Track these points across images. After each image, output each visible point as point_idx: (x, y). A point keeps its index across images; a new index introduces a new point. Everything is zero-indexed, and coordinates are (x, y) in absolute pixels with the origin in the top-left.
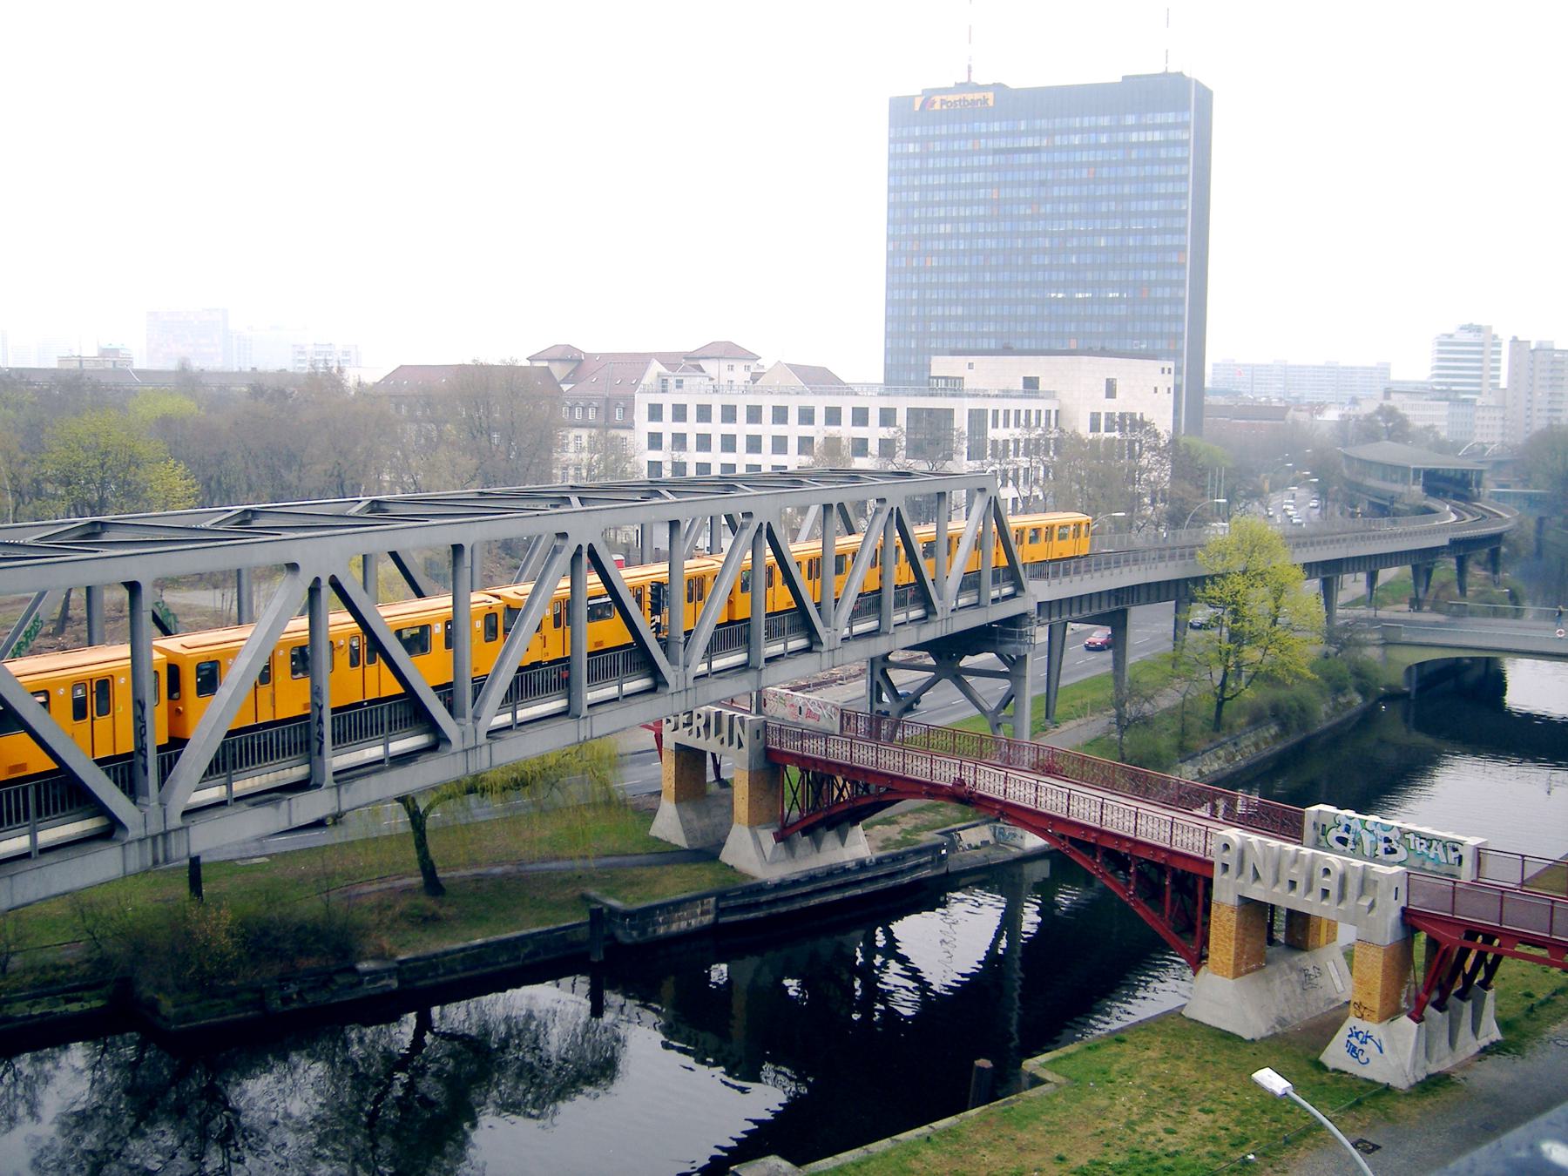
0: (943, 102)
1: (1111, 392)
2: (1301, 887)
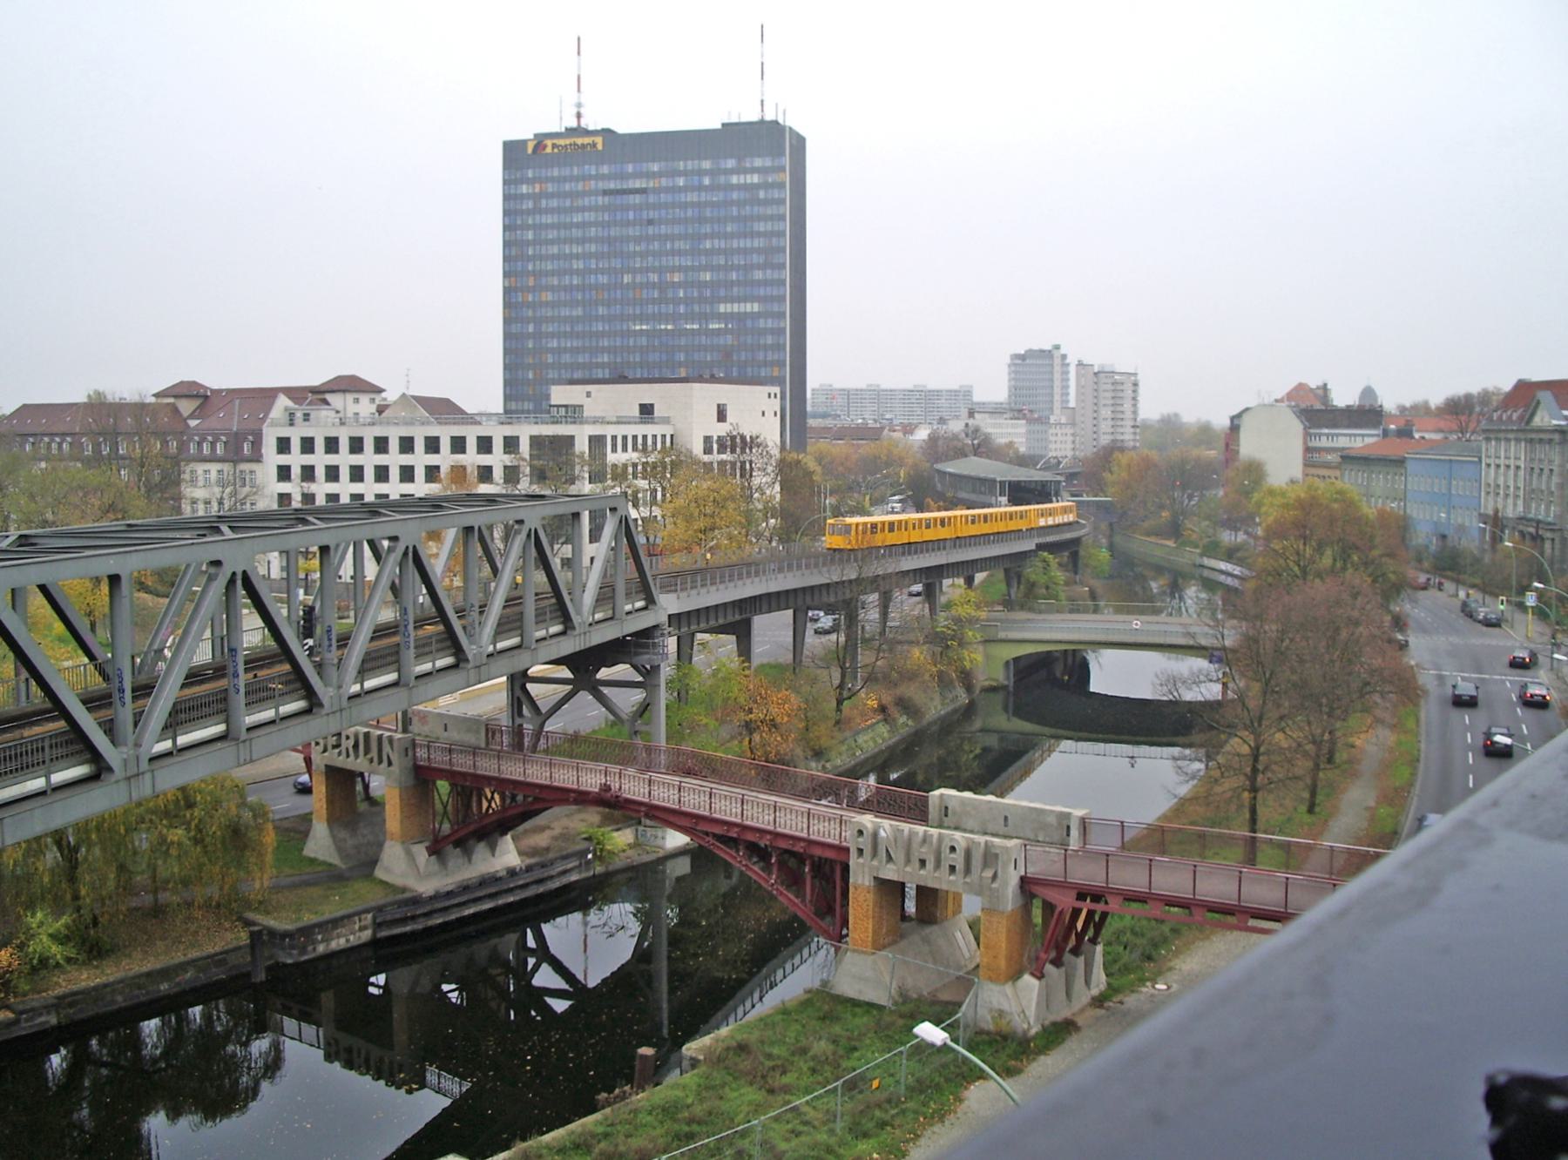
0: (554, 146)
1: (721, 416)
2: (930, 865)
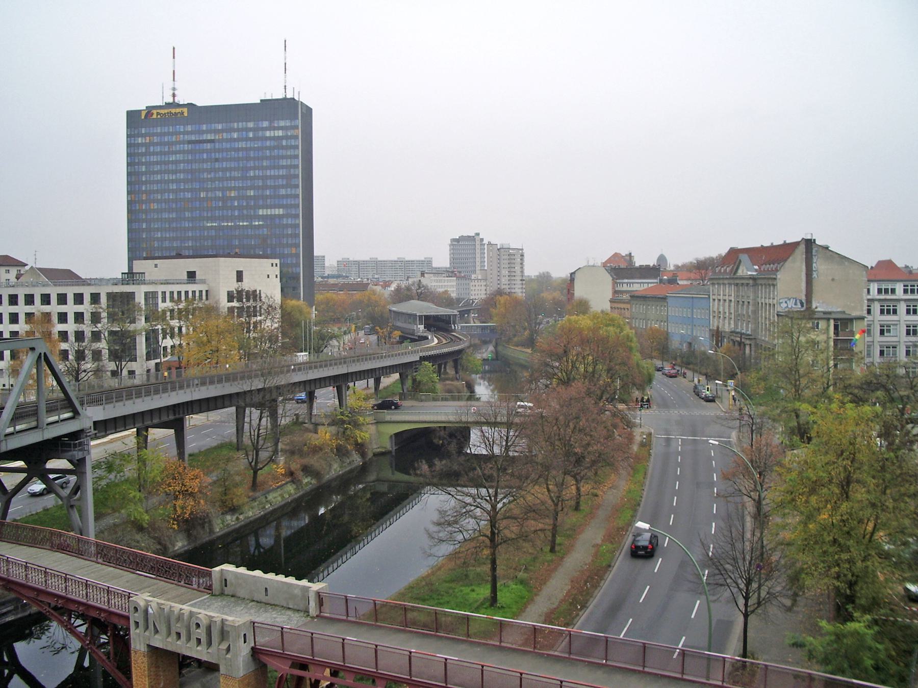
1: (240, 276)
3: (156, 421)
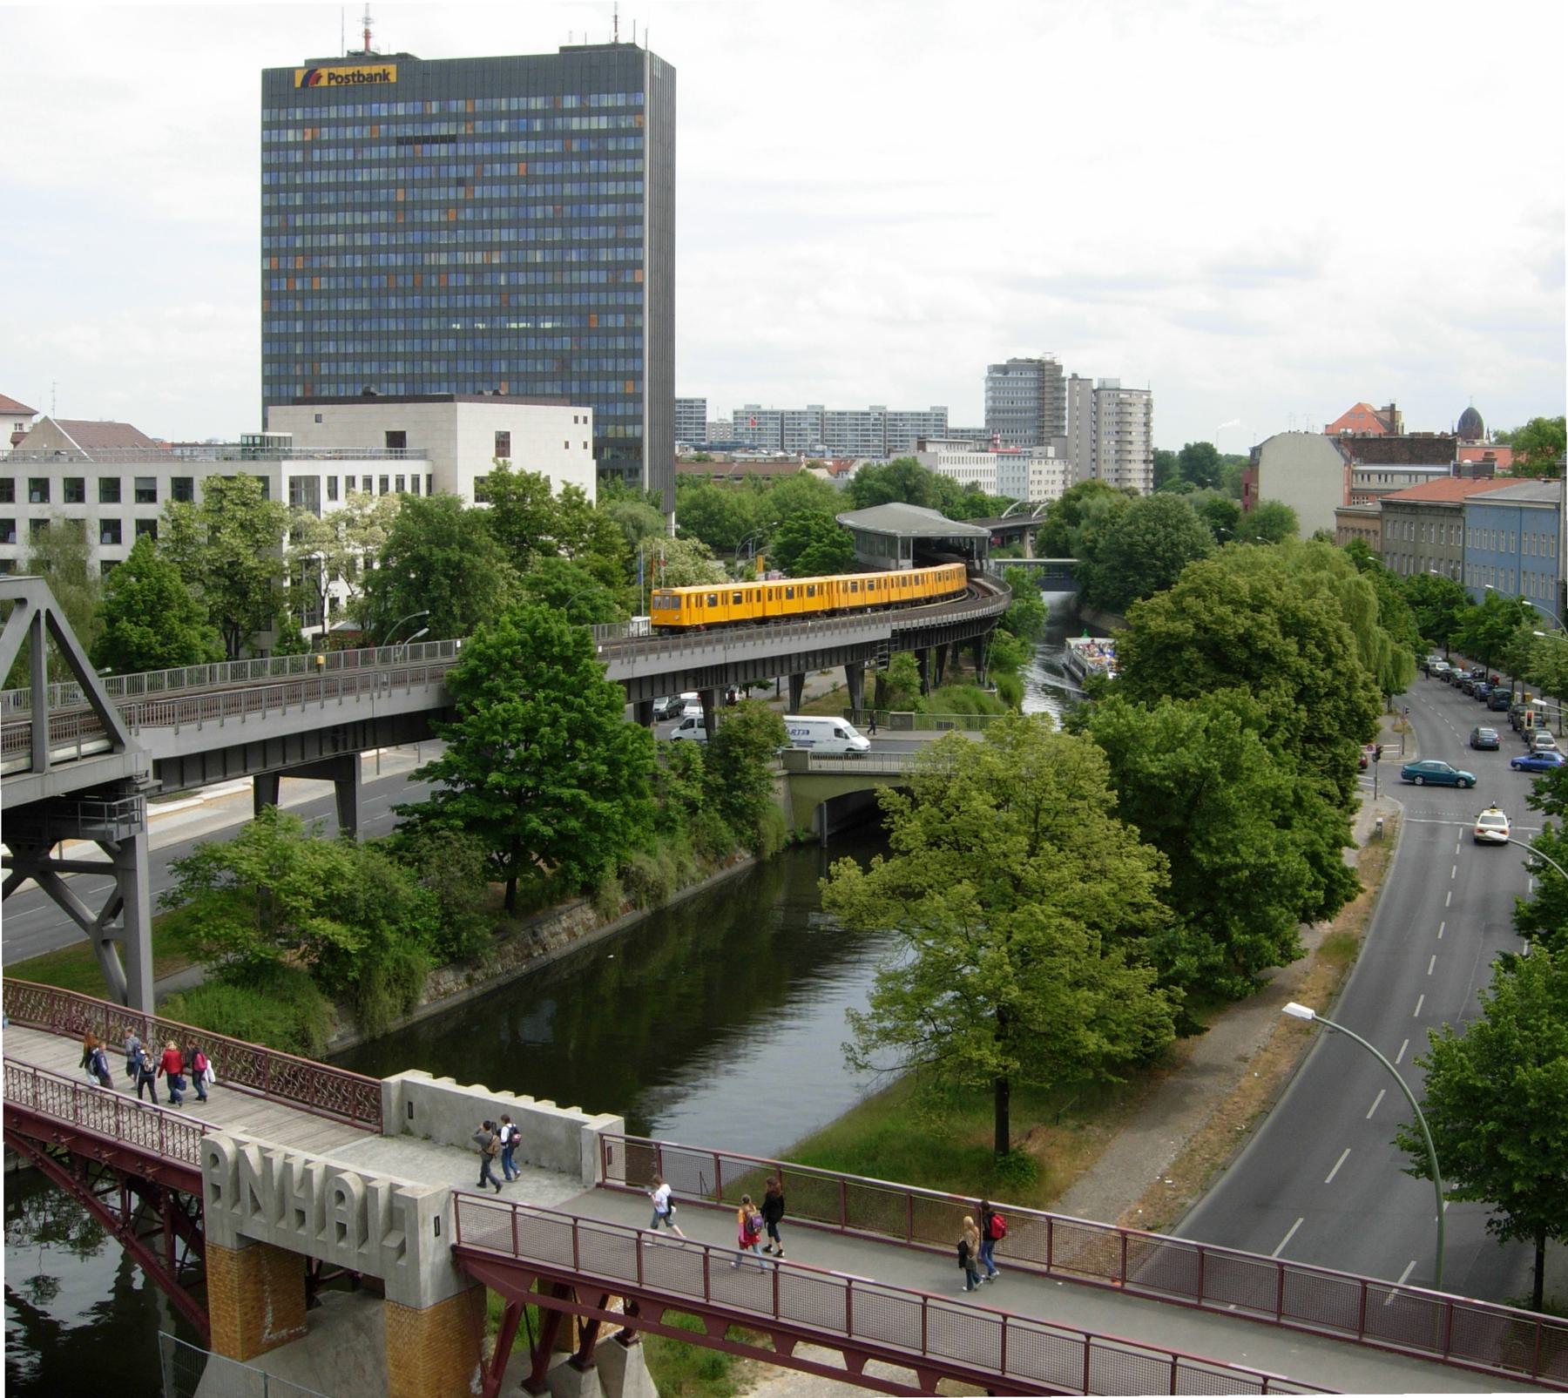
0: (331, 77)
1: (503, 444)
2: (311, 1221)
3: (292, 762)
